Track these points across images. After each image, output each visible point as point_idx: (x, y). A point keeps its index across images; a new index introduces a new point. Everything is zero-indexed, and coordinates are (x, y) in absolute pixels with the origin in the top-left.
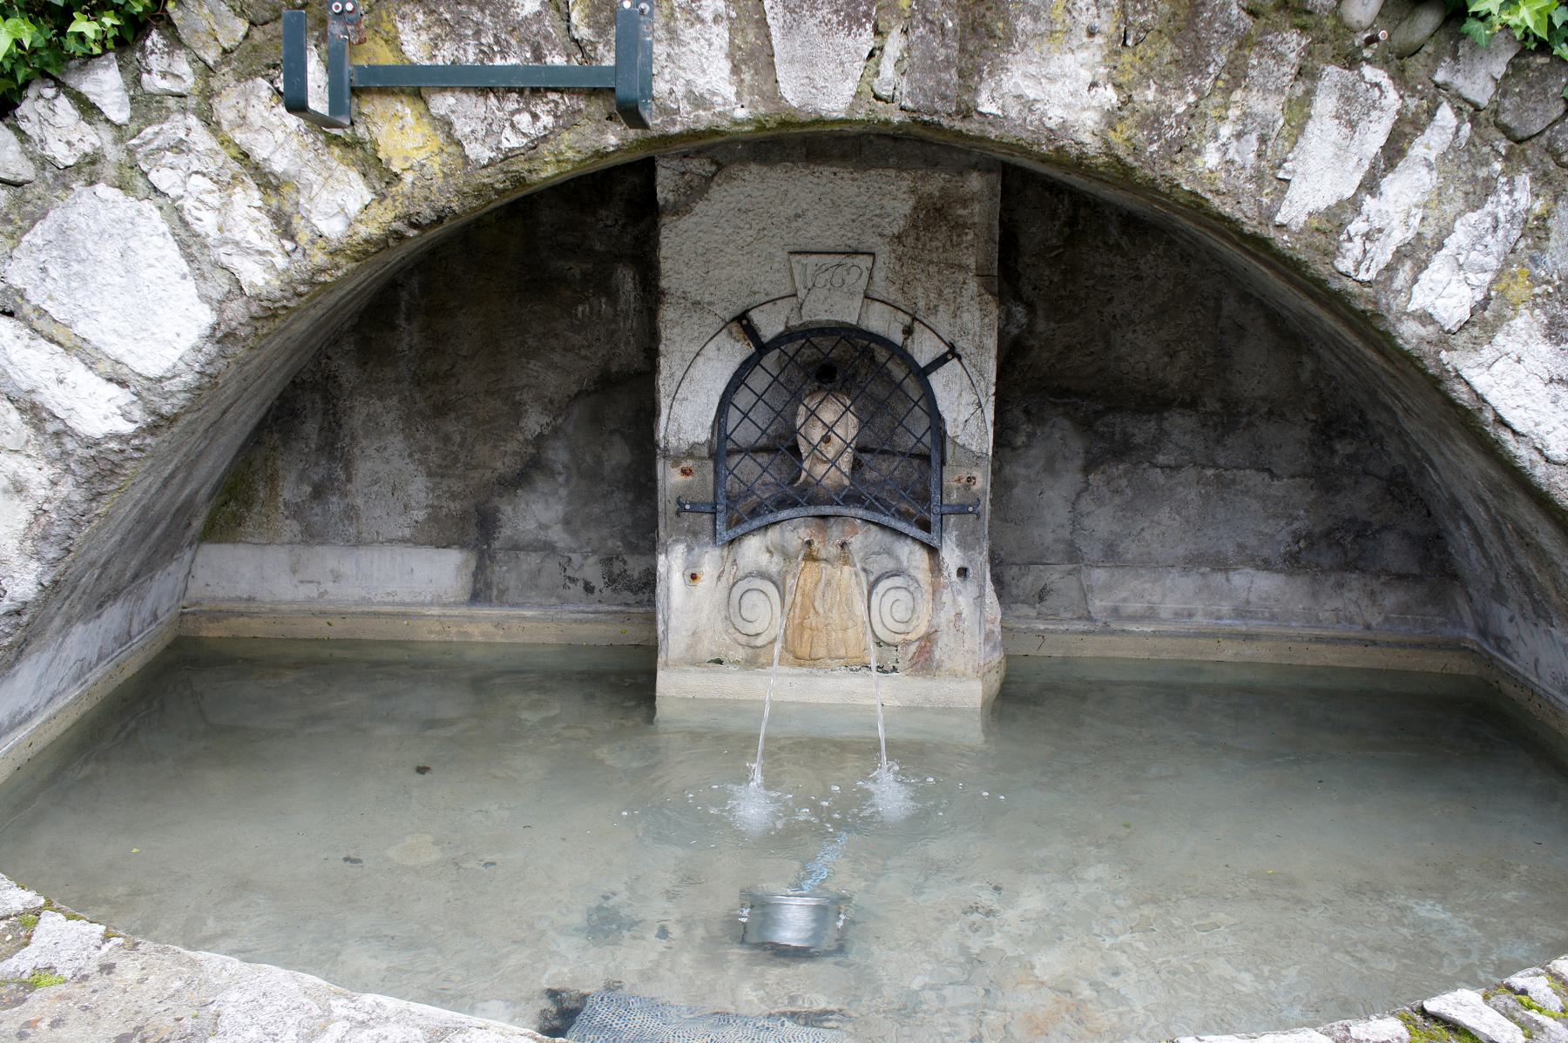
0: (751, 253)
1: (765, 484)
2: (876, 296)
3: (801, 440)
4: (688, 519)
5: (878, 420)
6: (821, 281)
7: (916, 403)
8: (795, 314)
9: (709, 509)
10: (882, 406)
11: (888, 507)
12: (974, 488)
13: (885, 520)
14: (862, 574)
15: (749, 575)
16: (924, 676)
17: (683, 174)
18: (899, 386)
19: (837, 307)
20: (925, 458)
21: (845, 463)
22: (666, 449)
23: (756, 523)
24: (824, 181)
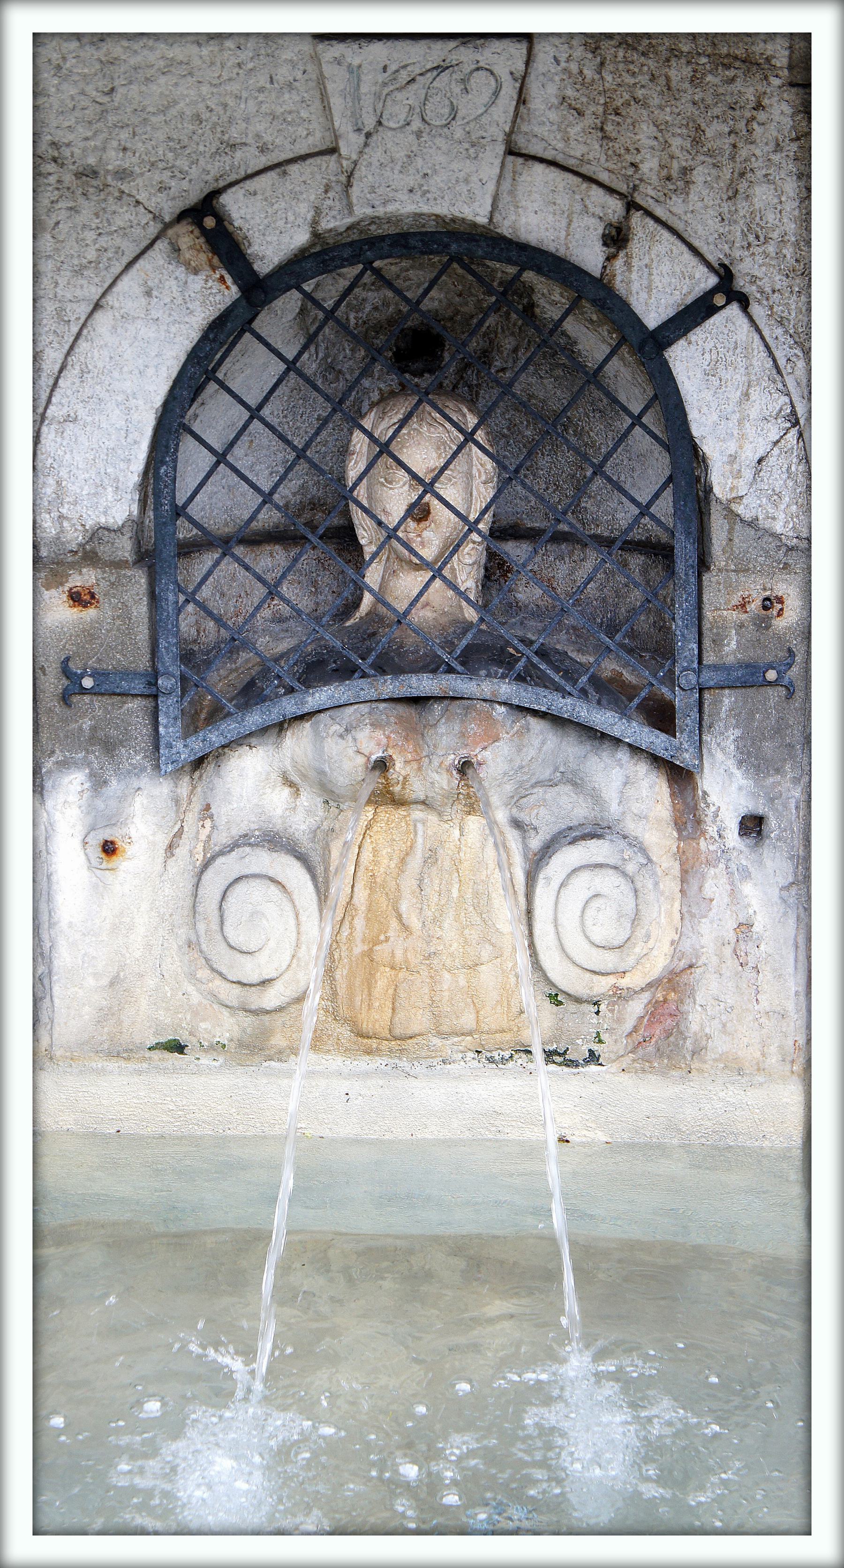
1: (279, 619)
2: (536, 148)
3: (359, 518)
5: (543, 461)
6: (396, 113)
7: (637, 420)
8: (333, 202)
9: (139, 686)
10: (553, 426)
11: (570, 675)
12: (780, 624)
13: (564, 705)
14: (512, 837)
15: (243, 841)
16: (663, 1073)
18: (596, 377)
19: (437, 181)
20: (660, 552)
21: (467, 570)
23: (254, 719)
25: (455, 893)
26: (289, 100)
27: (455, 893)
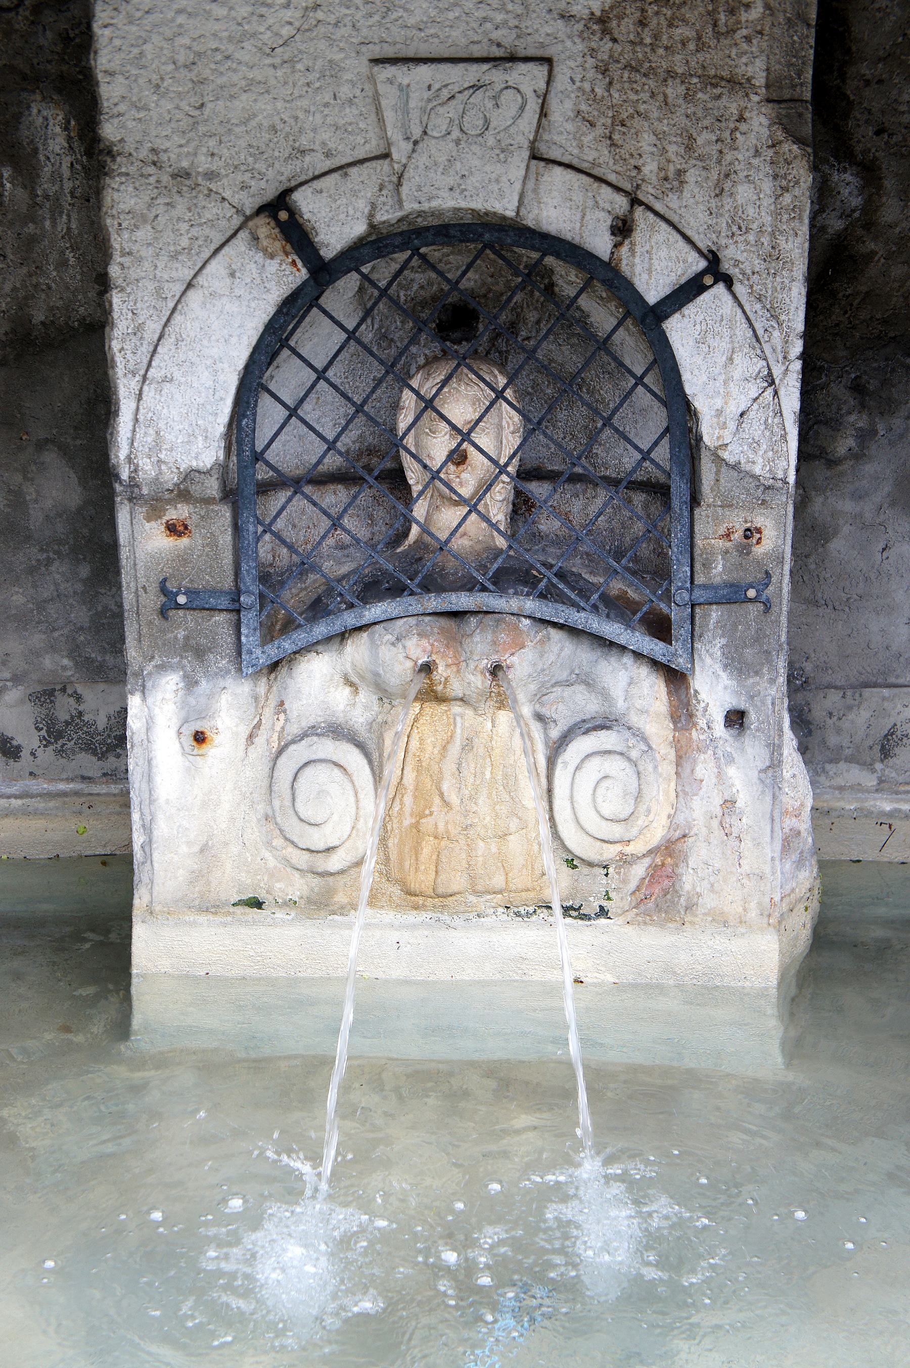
3: (407, 462)
4: (185, 624)
12: (758, 550)
18: (604, 344)
21: (498, 504)
22: (133, 484)
25: (488, 775)
26: (350, 113)
27: (488, 775)
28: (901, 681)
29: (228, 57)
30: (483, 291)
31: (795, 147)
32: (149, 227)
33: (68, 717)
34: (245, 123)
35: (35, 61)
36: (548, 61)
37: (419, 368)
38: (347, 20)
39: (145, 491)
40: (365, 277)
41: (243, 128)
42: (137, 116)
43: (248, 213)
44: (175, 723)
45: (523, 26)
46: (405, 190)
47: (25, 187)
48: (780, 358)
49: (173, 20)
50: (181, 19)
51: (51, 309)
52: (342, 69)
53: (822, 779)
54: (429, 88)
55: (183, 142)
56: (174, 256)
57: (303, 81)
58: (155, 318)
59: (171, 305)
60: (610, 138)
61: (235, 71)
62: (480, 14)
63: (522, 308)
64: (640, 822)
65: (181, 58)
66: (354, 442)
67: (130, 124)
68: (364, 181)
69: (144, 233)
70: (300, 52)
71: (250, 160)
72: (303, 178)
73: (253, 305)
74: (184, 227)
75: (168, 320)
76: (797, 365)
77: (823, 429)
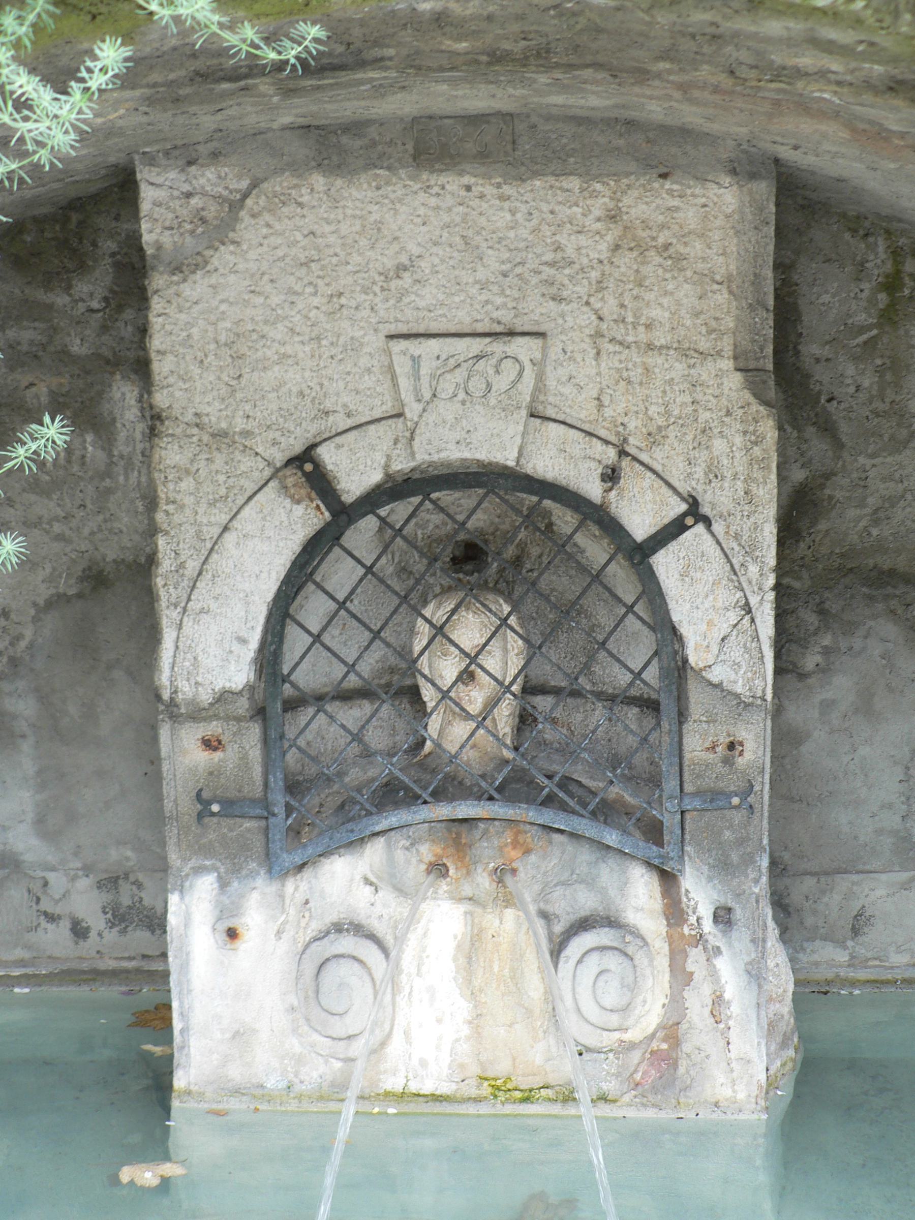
0: (318, 339)
2: (551, 412)
3: (421, 682)
4: (215, 830)
6: (447, 386)
12: (741, 762)
17: (189, 195)
18: (597, 577)
20: (650, 706)
21: (505, 716)
22: (173, 703)
23: (342, 836)
24: (449, 201)
26: (368, 381)
28: (868, 867)
29: (263, 337)
30: (491, 530)
31: (761, 408)
32: (191, 480)
33: (130, 903)
34: (276, 390)
35: (117, 349)
36: (542, 335)
37: (435, 596)
38: (367, 304)
39: (183, 711)
40: (382, 520)
41: (275, 394)
42: (184, 387)
43: (278, 465)
44: (210, 919)
45: (520, 307)
46: (416, 443)
47: (103, 449)
48: (756, 589)
49: (217, 308)
50: (223, 307)
51: (123, 548)
52: (362, 344)
53: (801, 956)
54: (438, 358)
55: (223, 407)
56: (212, 504)
57: (327, 354)
58: (195, 557)
59: (209, 545)
60: (598, 399)
61: (269, 347)
62: (483, 298)
63: (526, 544)
64: (637, 1012)
65: (222, 338)
66: (377, 662)
67: (178, 394)
68: (382, 435)
69: (187, 484)
70: (326, 330)
71: (281, 420)
72: (327, 435)
73: (281, 544)
74: (221, 478)
75: (207, 559)
76: (771, 596)
77: (794, 647)
